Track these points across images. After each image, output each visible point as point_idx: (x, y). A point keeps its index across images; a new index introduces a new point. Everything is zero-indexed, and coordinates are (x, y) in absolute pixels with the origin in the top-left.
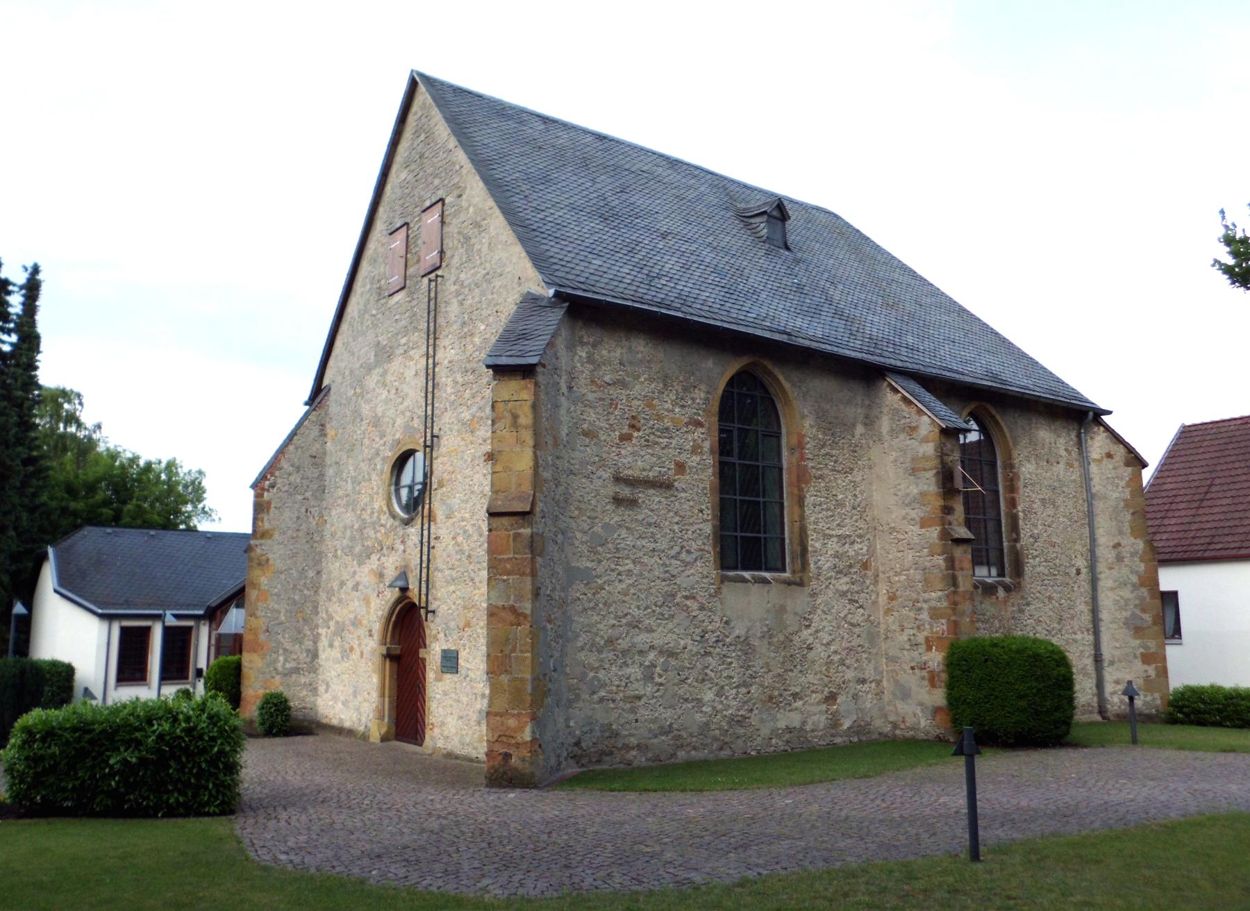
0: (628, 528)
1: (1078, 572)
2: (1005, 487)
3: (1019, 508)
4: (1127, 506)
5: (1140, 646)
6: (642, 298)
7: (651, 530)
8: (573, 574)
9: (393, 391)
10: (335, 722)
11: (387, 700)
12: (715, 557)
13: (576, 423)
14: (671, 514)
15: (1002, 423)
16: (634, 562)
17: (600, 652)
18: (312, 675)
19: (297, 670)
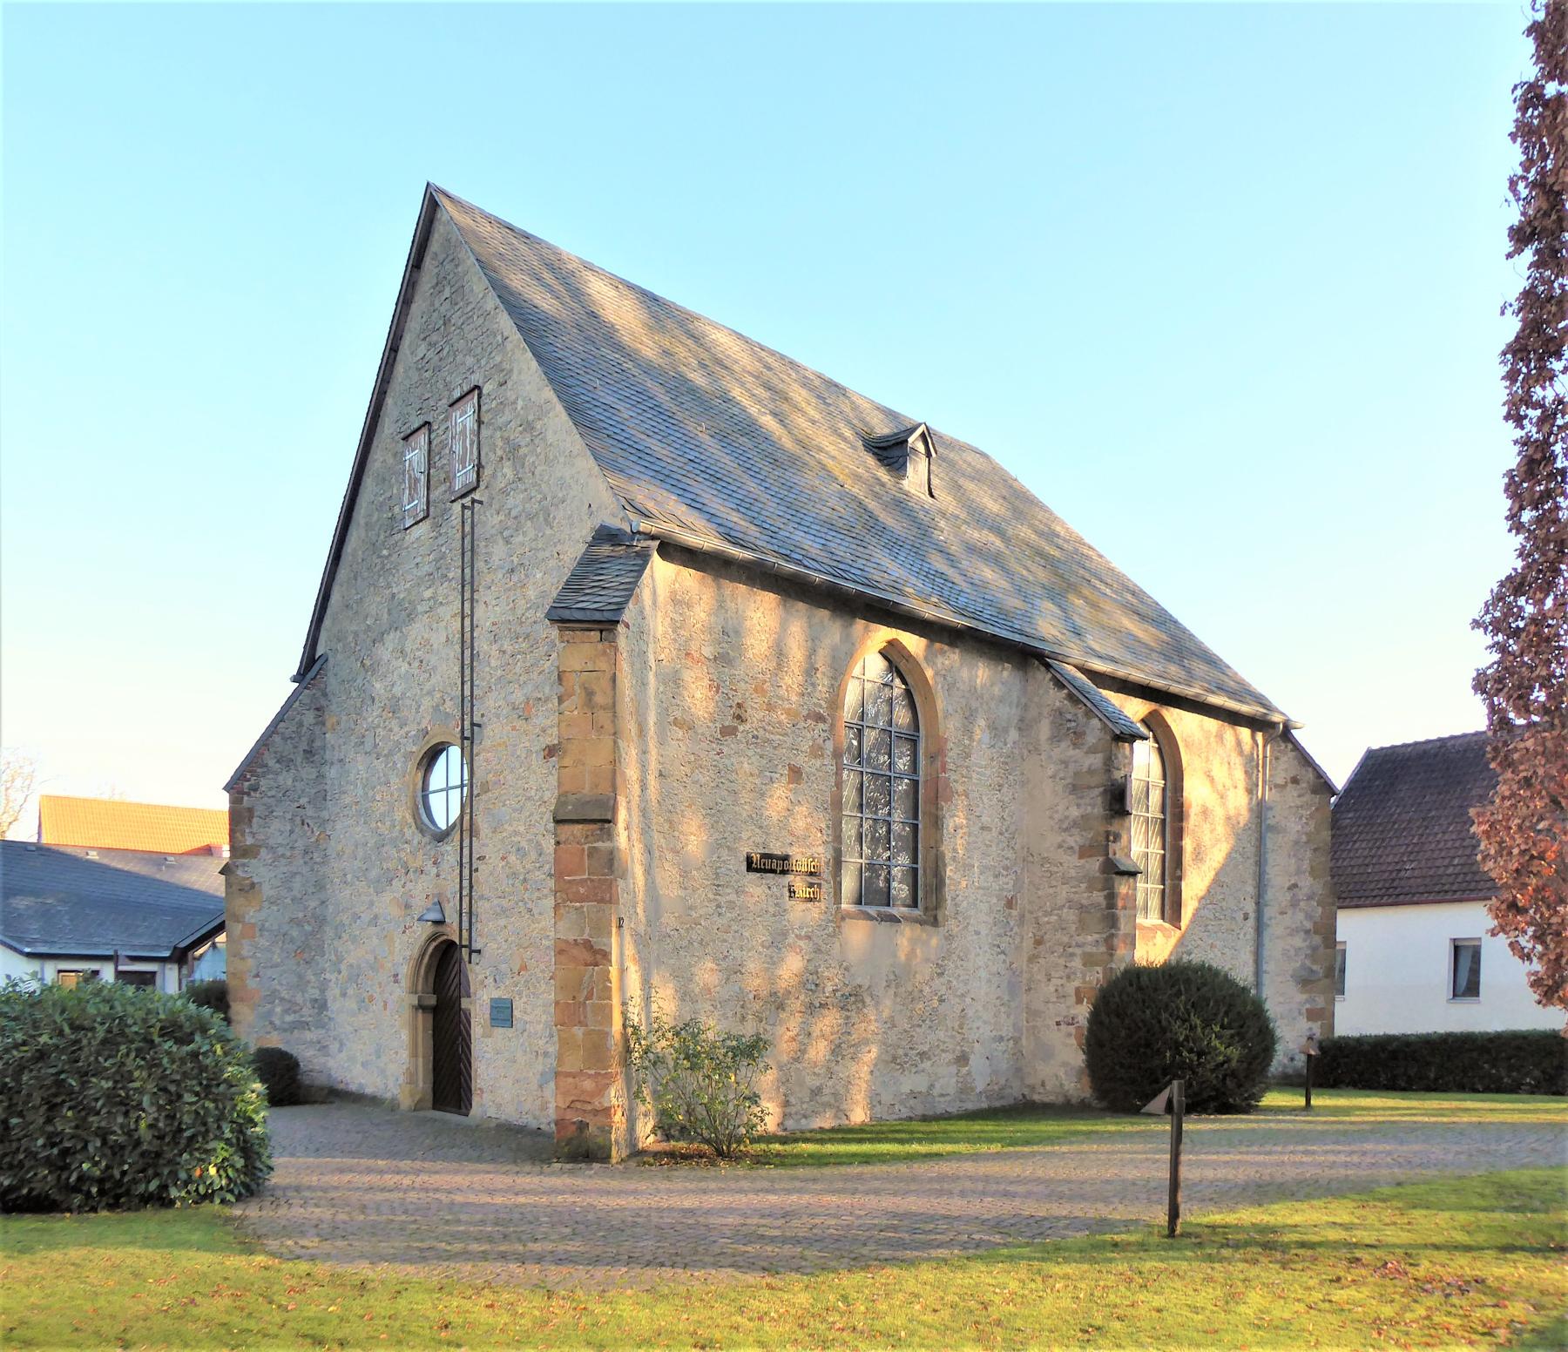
5: (1307, 1001)
9: (416, 664)
10: (353, 1087)
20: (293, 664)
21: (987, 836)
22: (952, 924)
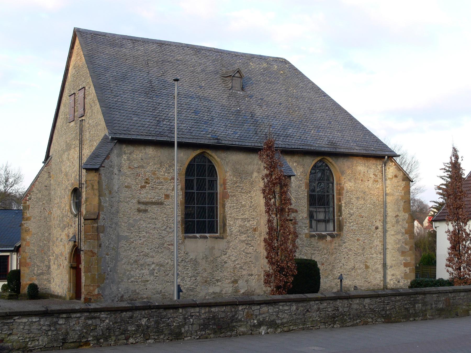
0: (143, 220)
1: (377, 228)
2: (337, 193)
3: (343, 202)
4: (402, 199)
5: (404, 260)
6: (150, 133)
7: (154, 220)
8: (119, 238)
9: (71, 163)
10: (56, 294)
11: (72, 284)
12: (182, 229)
13: (122, 183)
14: (163, 214)
15: (335, 165)
16: (146, 233)
17: (132, 265)
18: (48, 275)
19: (42, 274)
20: (43, 158)
22: (229, 238)
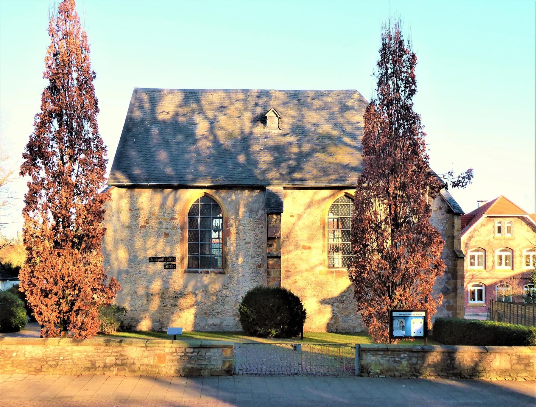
21: (248, 245)
22: (231, 273)
